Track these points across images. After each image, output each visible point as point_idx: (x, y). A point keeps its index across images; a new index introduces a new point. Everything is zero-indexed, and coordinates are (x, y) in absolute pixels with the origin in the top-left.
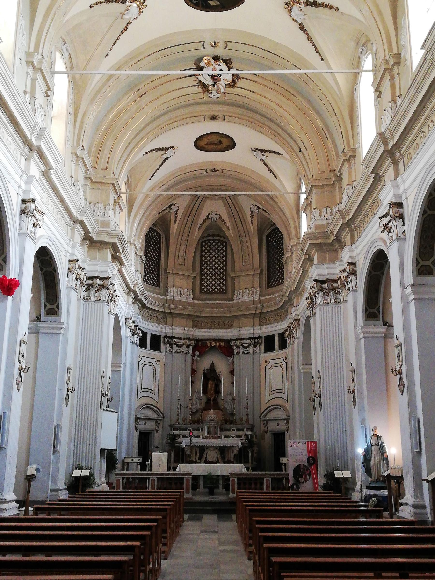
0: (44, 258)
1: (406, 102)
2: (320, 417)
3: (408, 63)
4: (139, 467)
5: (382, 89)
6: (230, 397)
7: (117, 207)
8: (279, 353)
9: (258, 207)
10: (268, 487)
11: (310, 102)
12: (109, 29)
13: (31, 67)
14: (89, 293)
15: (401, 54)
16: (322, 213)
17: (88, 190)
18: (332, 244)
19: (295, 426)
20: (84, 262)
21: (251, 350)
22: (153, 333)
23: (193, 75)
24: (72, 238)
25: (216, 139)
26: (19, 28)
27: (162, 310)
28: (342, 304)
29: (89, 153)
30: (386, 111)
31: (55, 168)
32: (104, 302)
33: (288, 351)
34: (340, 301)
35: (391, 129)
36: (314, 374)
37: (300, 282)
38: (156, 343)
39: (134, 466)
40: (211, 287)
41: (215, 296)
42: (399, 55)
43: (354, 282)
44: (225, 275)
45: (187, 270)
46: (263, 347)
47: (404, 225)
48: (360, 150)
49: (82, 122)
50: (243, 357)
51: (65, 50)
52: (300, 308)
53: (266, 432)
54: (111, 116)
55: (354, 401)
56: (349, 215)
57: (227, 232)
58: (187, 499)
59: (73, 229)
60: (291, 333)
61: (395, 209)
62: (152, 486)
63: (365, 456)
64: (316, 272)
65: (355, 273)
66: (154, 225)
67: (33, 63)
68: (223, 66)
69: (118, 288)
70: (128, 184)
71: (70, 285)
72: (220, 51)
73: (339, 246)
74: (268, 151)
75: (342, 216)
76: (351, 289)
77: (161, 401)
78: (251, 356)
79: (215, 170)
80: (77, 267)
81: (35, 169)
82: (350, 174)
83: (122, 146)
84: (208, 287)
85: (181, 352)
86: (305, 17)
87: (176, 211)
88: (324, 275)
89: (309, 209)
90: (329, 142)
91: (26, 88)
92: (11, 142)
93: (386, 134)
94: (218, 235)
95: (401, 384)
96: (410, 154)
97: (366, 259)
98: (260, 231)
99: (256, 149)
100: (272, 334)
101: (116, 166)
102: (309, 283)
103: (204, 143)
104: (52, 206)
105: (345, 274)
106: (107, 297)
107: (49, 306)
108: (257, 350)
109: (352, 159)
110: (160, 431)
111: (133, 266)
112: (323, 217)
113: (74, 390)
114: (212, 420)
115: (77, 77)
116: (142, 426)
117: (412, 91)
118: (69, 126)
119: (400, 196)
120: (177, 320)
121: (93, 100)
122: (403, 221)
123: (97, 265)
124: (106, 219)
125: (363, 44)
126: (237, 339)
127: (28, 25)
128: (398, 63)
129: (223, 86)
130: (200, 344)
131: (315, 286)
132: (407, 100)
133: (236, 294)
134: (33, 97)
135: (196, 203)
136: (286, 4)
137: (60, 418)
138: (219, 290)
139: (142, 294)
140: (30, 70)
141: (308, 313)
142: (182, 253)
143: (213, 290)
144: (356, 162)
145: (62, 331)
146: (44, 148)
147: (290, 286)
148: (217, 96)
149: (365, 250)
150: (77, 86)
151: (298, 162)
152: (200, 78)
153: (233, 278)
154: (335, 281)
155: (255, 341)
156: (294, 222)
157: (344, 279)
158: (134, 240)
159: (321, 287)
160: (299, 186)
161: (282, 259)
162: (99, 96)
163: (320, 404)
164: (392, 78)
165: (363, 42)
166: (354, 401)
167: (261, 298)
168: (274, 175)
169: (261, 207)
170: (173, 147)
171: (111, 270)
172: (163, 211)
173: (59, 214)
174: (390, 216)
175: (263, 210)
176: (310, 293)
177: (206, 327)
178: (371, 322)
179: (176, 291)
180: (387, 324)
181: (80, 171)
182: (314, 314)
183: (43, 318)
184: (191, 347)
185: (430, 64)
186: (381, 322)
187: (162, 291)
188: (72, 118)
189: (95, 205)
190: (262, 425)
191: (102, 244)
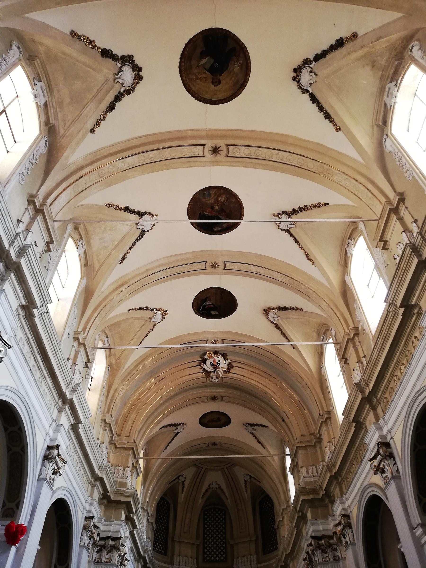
0: (60, 511)
5: (348, 356)
7: (134, 471)
9: (250, 476)
12: (141, 328)
13: (77, 342)
14: (100, 555)
15: (358, 328)
16: (309, 471)
17: (111, 455)
18: (322, 500)
20: (99, 521)
24: (92, 495)
26: (72, 313)
28: (341, 563)
30: (355, 370)
31: (83, 422)
34: (339, 558)
35: (365, 378)
40: (213, 556)
43: (350, 534)
47: (395, 463)
48: (335, 411)
49: (113, 396)
51: (106, 342)
54: (137, 395)
56: (335, 467)
64: (310, 529)
66: (165, 494)
67: (78, 338)
68: (221, 359)
69: (127, 547)
71: (82, 544)
73: (329, 501)
75: (329, 468)
76: (349, 542)
79: (215, 444)
80: (92, 524)
81: (65, 420)
82: (329, 433)
84: (210, 556)
86: (279, 318)
87: (184, 482)
88: (319, 531)
89: (296, 470)
90: (306, 411)
91: (70, 356)
92: (48, 393)
93: (361, 384)
96: (386, 398)
97: (359, 508)
99: (247, 424)
101: (136, 435)
102: (305, 544)
104: (76, 461)
105: (339, 528)
106: (117, 560)
109: (328, 420)
111: (145, 532)
112: (310, 474)
118: (102, 397)
119: (385, 437)
121: (124, 380)
122: (394, 460)
123: (111, 525)
124: (124, 480)
125: (323, 331)
127: (80, 315)
128: (357, 334)
129: (221, 372)
131: (313, 542)
132: (376, 350)
133: (235, 563)
134: (74, 364)
136: (264, 310)
138: (220, 558)
140: (76, 344)
143: (215, 558)
144: (332, 423)
146: (75, 401)
147: (285, 549)
148: (217, 380)
149: (357, 499)
150: (112, 369)
153: (232, 546)
154: (331, 538)
156: (282, 486)
157: (340, 533)
158: (147, 507)
159: (318, 544)
161: (274, 524)
162: (128, 377)
164: (355, 346)
165: (323, 331)
167: (259, 565)
168: (262, 446)
169: (253, 476)
170: (183, 423)
171: (124, 532)
172: (173, 481)
173: (82, 470)
174: (381, 455)
175: (255, 478)
176: (308, 553)
179: (181, 560)
181: (106, 435)
185: (393, 315)
189: (116, 466)
191: (119, 502)
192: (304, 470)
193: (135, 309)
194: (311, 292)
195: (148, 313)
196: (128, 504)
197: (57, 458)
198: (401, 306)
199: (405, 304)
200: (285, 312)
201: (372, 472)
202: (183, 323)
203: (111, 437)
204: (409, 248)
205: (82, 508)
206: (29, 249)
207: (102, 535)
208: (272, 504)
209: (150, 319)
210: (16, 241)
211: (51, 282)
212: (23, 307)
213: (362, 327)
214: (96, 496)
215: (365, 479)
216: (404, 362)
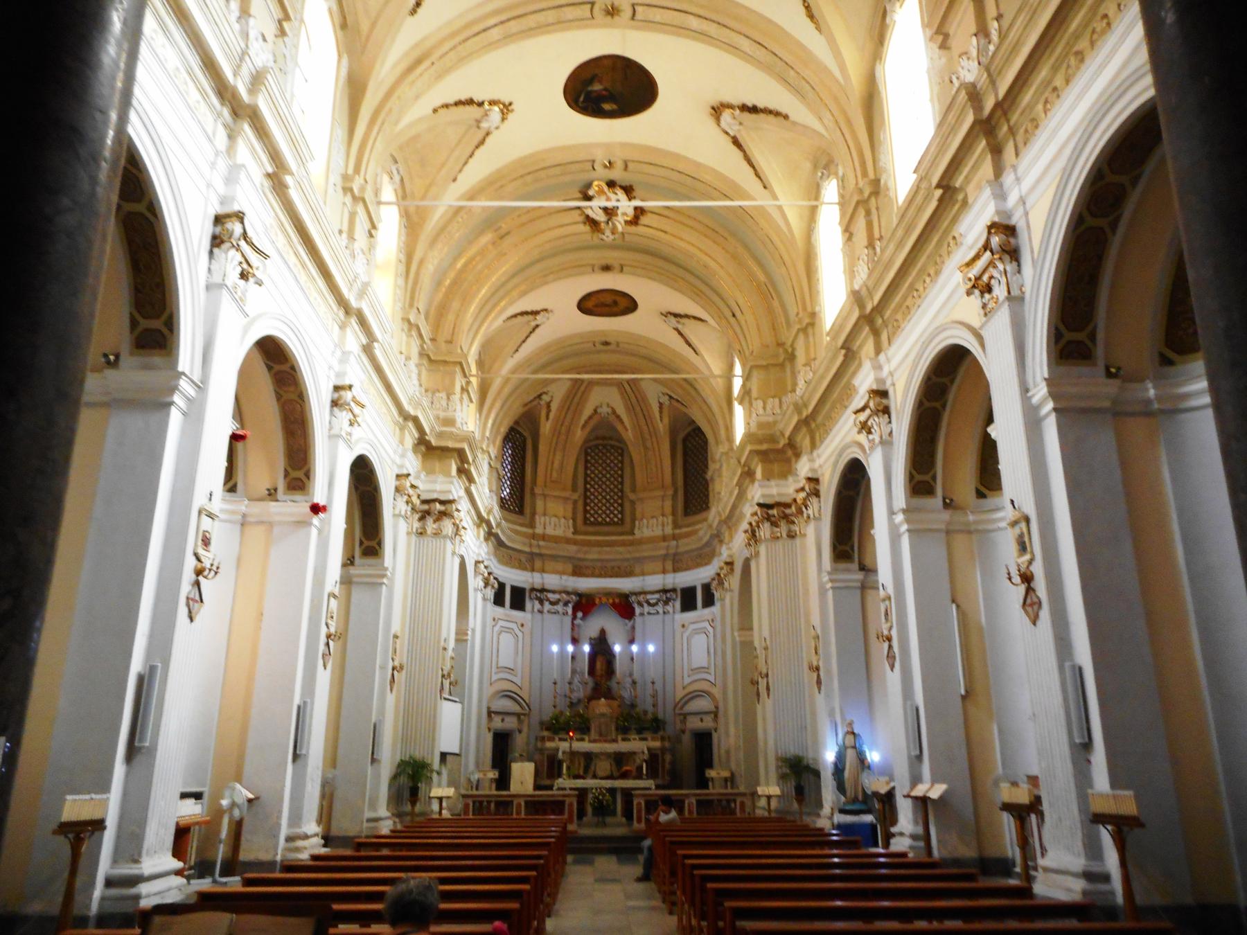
0: (362, 472)
1: (892, 247)
2: (767, 710)
3: (892, 194)
4: (494, 786)
5: (854, 229)
6: (629, 680)
7: (465, 396)
8: (701, 613)
10: (690, 812)
11: (746, 246)
17: (424, 372)
18: (781, 451)
19: (727, 724)
20: (417, 477)
21: (660, 608)
22: (515, 584)
23: (579, 208)
25: (608, 299)
27: (527, 549)
28: (798, 541)
29: (426, 318)
32: (445, 537)
33: (715, 609)
36: (756, 644)
37: (734, 507)
38: (518, 599)
39: (487, 784)
41: (606, 529)
42: (876, 182)
44: (621, 498)
45: (564, 489)
46: (678, 604)
49: (418, 273)
50: (647, 617)
51: (395, 172)
52: (736, 545)
53: (683, 732)
54: (459, 265)
55: (819, 682)
57: (624, 436)
58: (571, 832)
59: (402, 429)
60: (721, 583)
61: (878, 399)
62: (519, 812)
63: (836, 765)
64: (758, 492)
65: (816, 494)
66: (516, 423)
67: (351, 190)
68: (621, 195)
70: (480, 364)
72: (617, 174)
74: (687, 316)
75: (798, 408)
77: (526, 686)
78: (660, 617)
79: (606, 343)
81: (353, 339)
83: (473, 308)
85: (556, 613)
88: (773, 496)
90: (776, 303)
94: (611, 438)
95: (891, 657)
98: (673, 433)
100: (691, 584)
102: (749, 511)
103: (592, 304)
105: (802, 495)
107: (366, 543)
108: (669, 608)
110: (525, 729)
113: (402, 667)
114: (603, 715)
115: (412, 210)
116: (498, 723)
117: (900, 233)
120: (550, 565)
123: (435, 482)
125: (824, 164)
126: (640, 593)
127: (346, 137)
130: (584, 601)
134: (351, 237)
135: (578, 391)
136: (713, 108)
137: (382, 711)
139: (498, 525)
140: (348, 199)
141: (746, 553)
142: (557, 464)
145: (385, 581)
150: (412, 223)
151: (731, 332)
152: (589, 212)
154: (788, 506)
155: (666, 594)
156: (724, 418)
158: (488, 446)
160: (731, 367)
163: (768, 689)
164: (868, 213)
166: (819, 682)
171: (456, 490)
176: (751, 524)
177: (593, 575)
178: (842, 566)
180: (868, 569)
181: (413, 344)
182: (757, 554)
183: (357, 560)
184: (570, 605)
186: (855, 566)
187: (527, 521)
188: (402, 268)
189: (433, 393)
190: (678, 722)
191: (445, 451)
192: (760, 404)
193: (446, 106)
194: (808, 87)
195: (473, 111)
196: (461, 454)
197: (352, 404)
198: (938, 186)
199: (944, 183)
200: (754, 116)
201: (856, 430)
202: (546, 124)
203: (422, 346)
204: (963, 92)
205: (389, 462)
206: (269, 77)
207: (424, 497)
208: (706, 442)
209: (478, 122)
210: (244, 64)
211: (292, 95)
212: (269, 175)
213: (886, 184)
214: (409, 442)
215: (938, 312)
216: (932, 272)
